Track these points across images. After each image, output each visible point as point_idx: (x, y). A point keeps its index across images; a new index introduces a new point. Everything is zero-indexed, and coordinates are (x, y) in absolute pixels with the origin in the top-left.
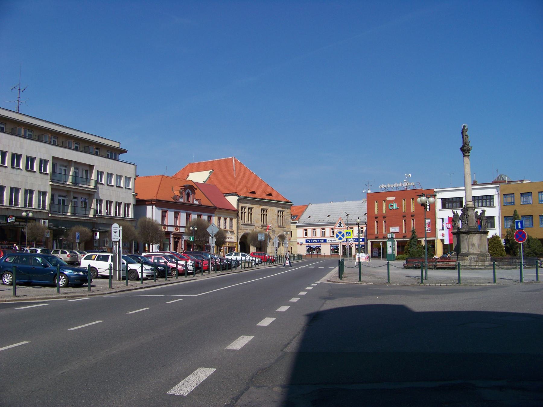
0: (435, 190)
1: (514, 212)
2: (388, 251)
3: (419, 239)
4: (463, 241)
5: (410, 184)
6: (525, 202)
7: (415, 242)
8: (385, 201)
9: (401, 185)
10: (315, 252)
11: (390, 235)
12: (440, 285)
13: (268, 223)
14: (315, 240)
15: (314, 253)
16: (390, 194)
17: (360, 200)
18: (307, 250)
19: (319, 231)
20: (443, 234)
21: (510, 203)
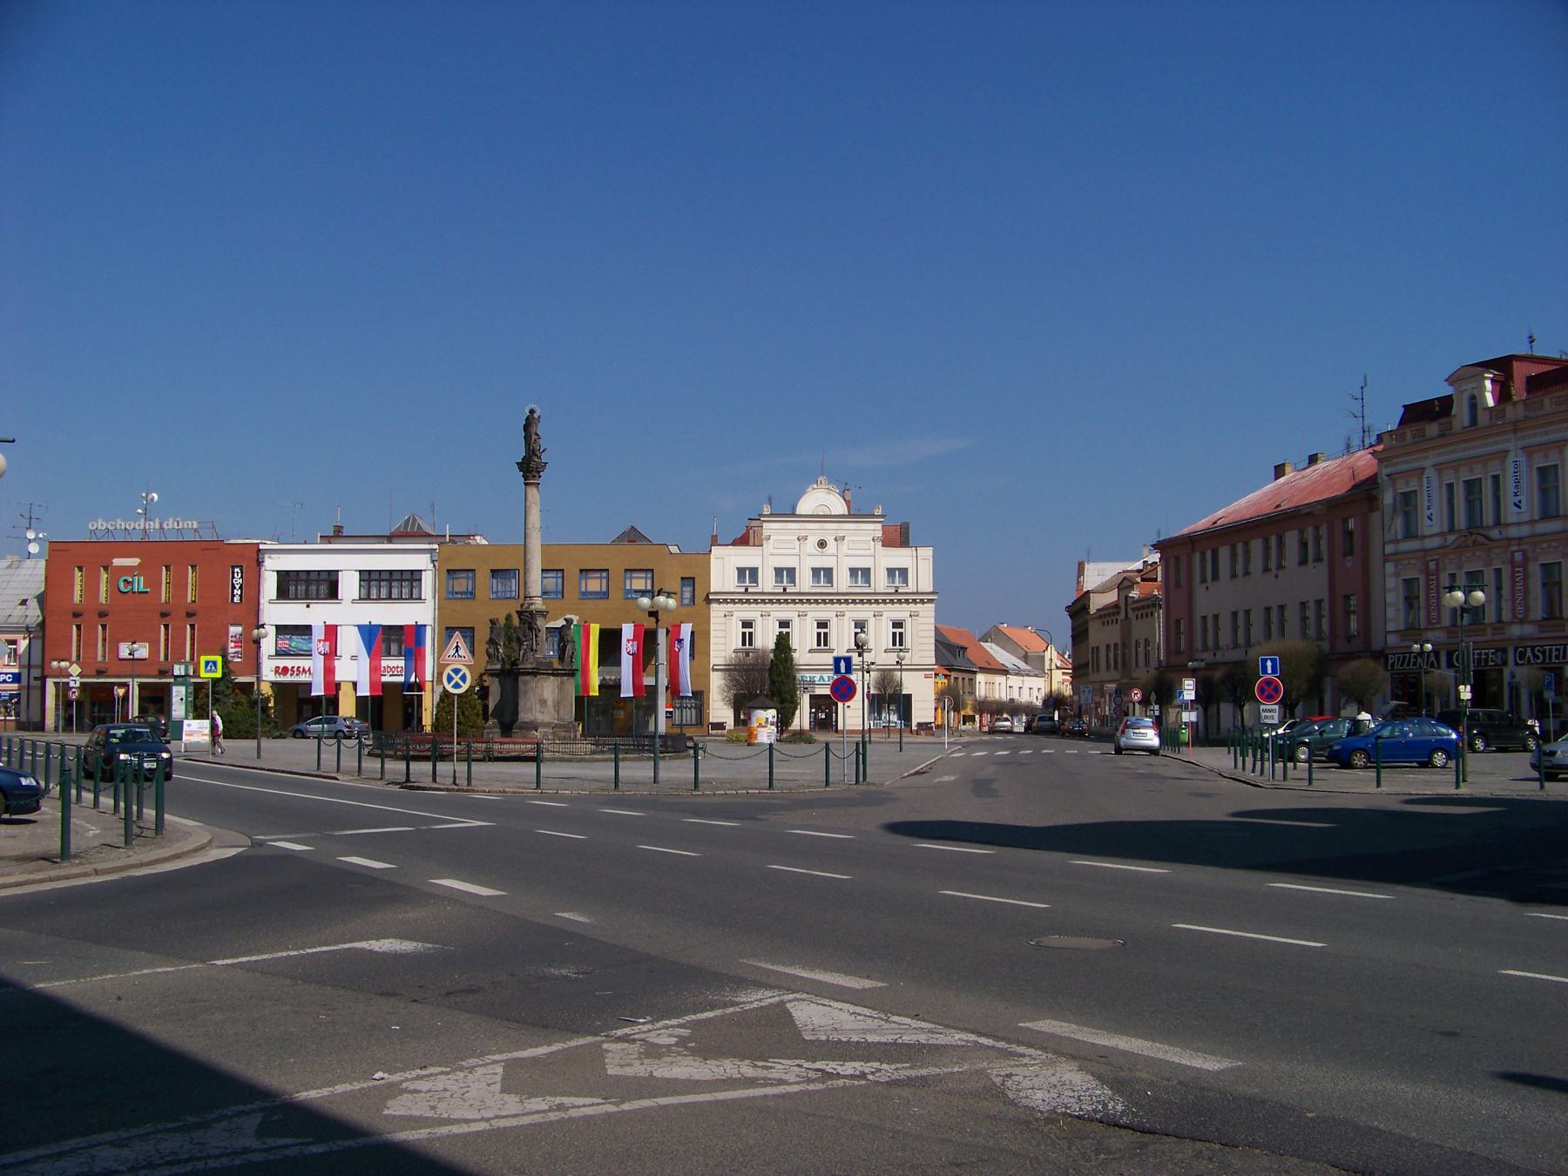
0: (261, 547)
1: (507, 619)
2: (173, 713)
3: (594, 692)
4: (525, 693)
5: (185, 524)
6: (499, 594)
7: (228, 687)
8: (106, 568)
9: (157, 526)
11: (183, 667)
12: (714, 794)
16: (126, 548)
20: (277, 667)
21: (461, 593)
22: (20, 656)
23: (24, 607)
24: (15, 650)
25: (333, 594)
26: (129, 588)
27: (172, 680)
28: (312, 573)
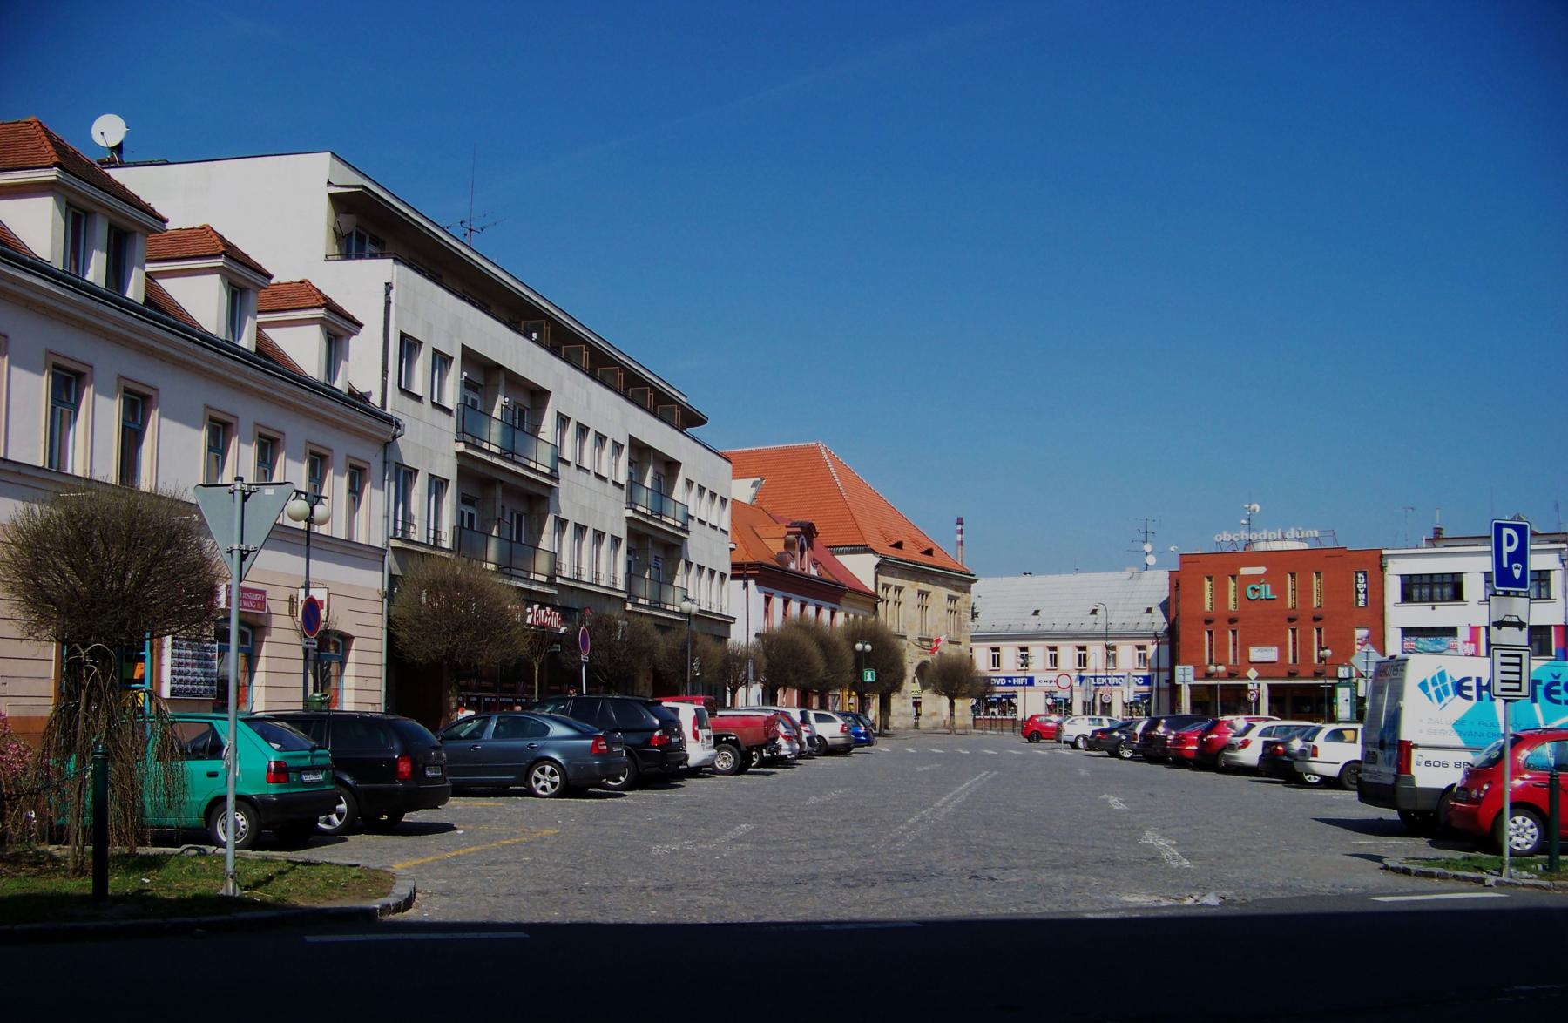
0: (1384, 552)
8: (1234, 577)
10: (996, 711)
13: (931, 630)
14: (998, 678)
15: (993, 713)
17: (1122, 569)
18: (973, 707)
19: (1009, 653)
22: (1149, 660)
23: (1150, 615)
24: (1145, 654)
25: (1457, 595)
26: (1257, 595)
27: (1336, 681)
28: (1424, 577)
